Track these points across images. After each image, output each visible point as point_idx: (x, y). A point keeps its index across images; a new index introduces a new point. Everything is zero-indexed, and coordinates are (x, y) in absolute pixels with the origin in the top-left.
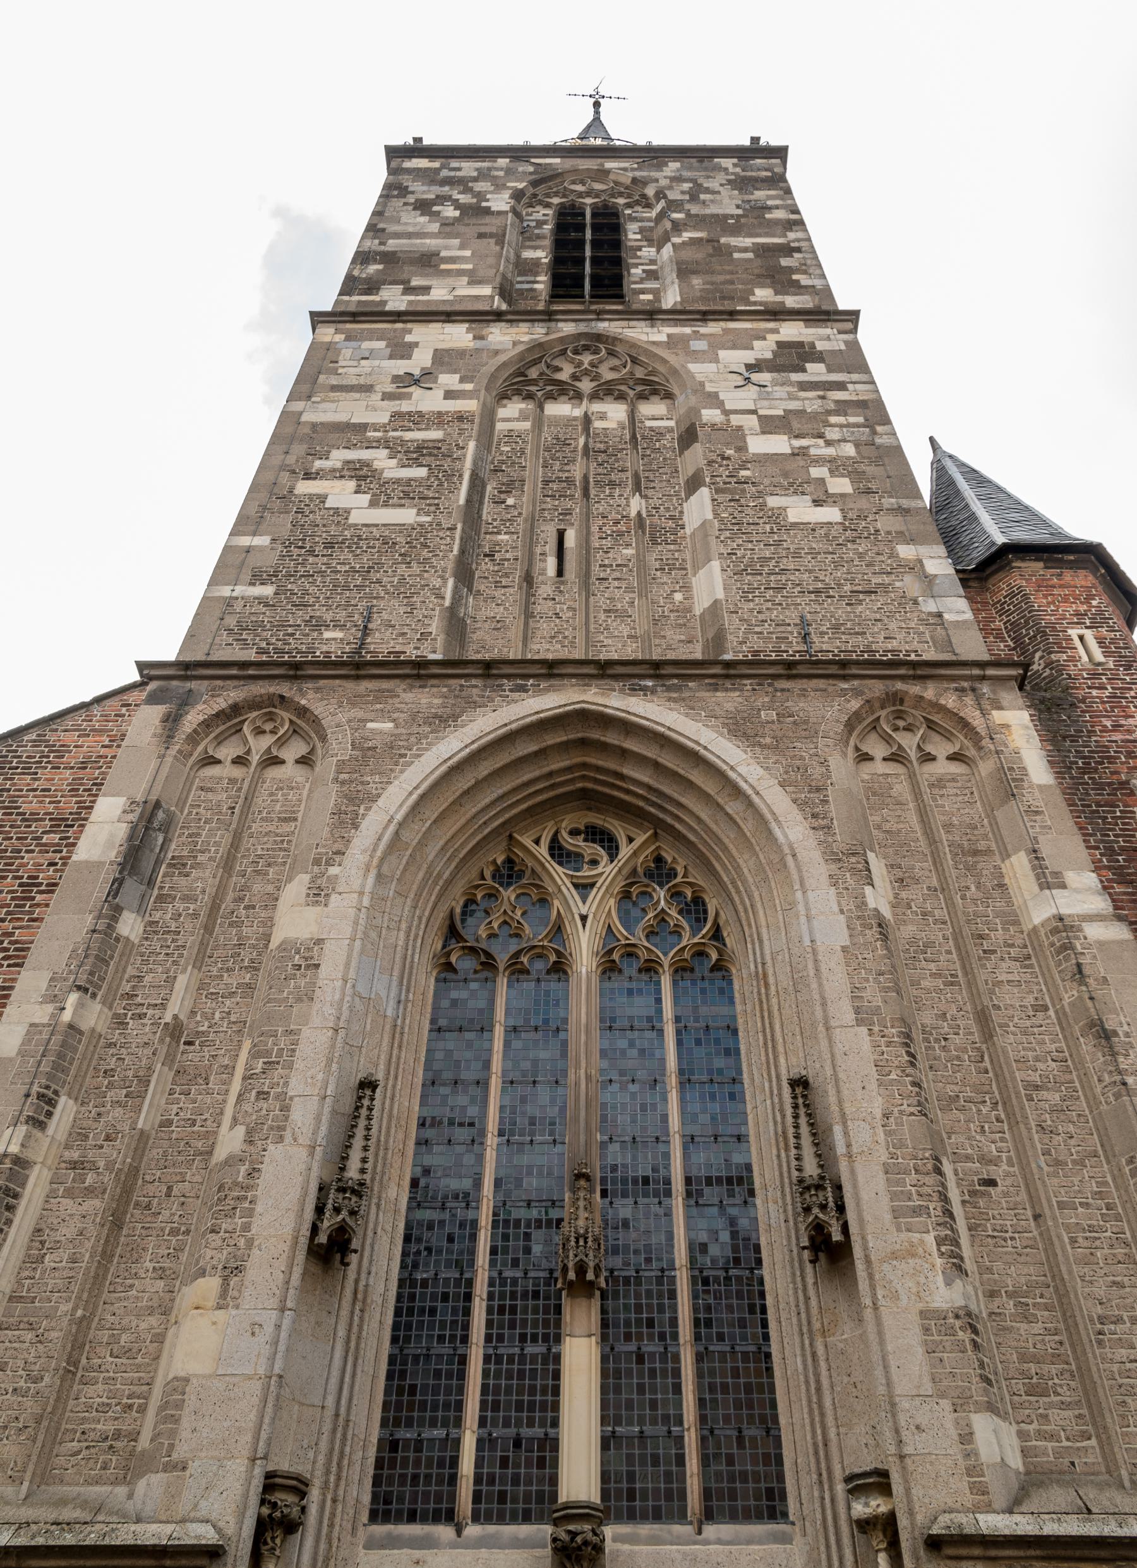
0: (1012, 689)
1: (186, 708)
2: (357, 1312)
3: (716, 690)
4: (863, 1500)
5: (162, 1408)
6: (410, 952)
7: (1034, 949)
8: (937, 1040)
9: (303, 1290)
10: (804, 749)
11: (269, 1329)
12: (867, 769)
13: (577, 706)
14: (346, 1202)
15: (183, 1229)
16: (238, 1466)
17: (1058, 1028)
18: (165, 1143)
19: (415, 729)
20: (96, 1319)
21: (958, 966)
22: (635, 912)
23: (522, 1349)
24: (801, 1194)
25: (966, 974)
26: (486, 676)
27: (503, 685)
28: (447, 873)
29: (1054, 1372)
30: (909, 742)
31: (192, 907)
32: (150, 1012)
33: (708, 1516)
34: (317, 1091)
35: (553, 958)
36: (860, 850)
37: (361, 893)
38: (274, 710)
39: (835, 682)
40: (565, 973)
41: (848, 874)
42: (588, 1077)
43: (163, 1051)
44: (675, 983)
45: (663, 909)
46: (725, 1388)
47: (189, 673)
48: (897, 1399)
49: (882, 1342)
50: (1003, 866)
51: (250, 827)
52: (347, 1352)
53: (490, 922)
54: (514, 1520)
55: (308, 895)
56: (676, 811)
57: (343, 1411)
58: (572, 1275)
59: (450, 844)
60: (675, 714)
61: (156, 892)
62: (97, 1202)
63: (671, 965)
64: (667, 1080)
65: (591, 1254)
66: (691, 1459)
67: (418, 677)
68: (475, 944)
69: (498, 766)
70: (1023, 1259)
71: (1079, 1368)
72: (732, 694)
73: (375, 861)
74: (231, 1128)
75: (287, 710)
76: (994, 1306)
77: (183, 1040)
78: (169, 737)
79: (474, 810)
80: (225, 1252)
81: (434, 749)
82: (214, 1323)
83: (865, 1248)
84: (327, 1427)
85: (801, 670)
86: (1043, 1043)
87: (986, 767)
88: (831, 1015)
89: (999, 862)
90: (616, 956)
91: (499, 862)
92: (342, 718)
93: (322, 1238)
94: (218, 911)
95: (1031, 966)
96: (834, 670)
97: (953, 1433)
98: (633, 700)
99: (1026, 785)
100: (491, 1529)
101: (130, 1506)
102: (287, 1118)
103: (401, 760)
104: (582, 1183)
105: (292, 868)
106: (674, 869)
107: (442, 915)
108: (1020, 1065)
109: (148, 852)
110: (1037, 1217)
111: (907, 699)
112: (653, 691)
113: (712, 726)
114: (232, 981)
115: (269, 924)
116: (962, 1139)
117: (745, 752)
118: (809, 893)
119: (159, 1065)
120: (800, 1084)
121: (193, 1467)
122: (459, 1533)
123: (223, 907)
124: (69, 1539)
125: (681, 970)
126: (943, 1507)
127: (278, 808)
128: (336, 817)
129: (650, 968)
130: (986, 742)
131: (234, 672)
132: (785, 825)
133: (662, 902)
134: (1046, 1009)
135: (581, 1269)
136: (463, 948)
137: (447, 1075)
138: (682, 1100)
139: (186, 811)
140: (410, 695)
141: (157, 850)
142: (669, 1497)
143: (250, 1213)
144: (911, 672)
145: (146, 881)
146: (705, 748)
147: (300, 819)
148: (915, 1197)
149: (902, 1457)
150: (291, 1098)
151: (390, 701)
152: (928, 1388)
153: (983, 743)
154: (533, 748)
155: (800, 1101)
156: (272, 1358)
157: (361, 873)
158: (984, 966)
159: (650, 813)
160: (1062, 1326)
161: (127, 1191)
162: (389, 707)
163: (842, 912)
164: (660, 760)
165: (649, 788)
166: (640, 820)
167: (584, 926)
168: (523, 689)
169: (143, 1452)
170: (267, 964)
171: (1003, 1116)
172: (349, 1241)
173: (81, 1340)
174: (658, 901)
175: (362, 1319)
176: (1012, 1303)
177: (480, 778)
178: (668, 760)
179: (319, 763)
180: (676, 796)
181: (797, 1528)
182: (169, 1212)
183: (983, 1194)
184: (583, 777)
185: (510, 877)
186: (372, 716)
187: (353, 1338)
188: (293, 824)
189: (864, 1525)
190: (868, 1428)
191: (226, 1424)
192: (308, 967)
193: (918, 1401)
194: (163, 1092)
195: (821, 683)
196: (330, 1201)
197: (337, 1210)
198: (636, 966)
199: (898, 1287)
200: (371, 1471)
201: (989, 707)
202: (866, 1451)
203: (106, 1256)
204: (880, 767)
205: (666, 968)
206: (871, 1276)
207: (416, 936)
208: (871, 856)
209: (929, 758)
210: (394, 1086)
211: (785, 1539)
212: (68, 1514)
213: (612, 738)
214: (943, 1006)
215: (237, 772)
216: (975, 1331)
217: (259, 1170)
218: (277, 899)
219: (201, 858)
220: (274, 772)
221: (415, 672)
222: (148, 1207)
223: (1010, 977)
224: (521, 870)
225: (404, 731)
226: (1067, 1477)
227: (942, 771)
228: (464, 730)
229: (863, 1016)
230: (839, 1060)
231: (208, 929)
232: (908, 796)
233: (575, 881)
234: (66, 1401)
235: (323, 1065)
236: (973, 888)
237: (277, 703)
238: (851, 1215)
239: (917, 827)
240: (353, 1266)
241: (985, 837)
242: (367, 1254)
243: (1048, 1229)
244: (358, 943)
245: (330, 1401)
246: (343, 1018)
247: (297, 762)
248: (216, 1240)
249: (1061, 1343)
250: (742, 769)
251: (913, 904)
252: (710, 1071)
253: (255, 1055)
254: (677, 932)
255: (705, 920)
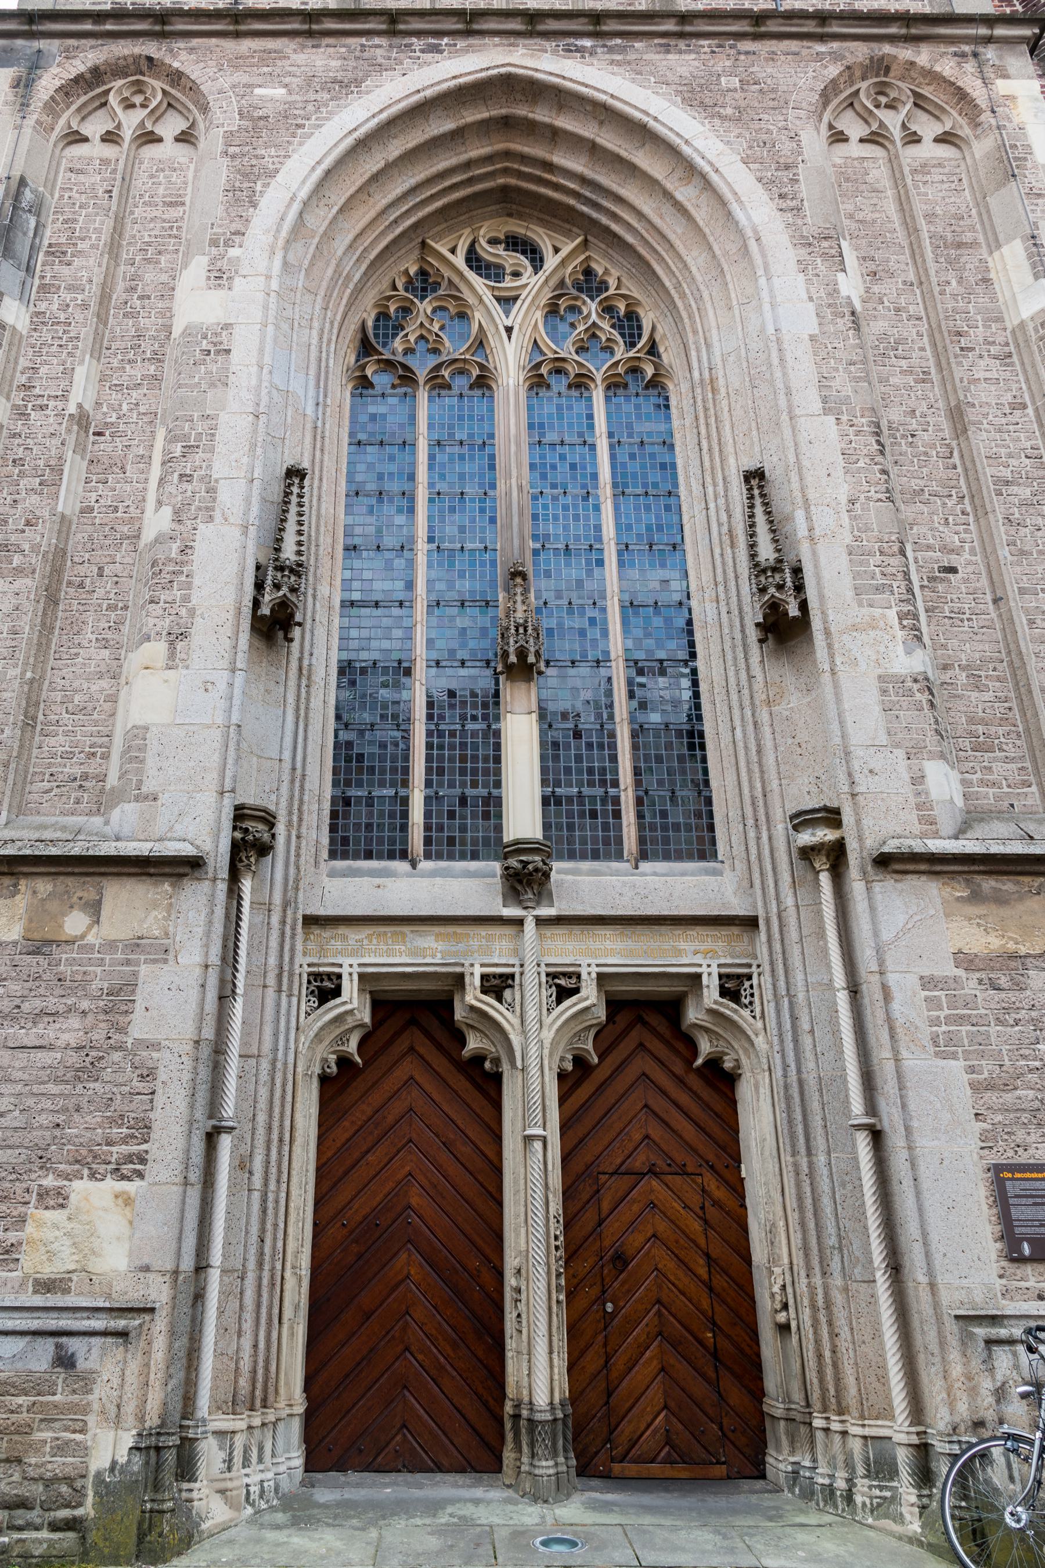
0: (1022, 54)
1: (38, 72)
2: (303, 685)
3: (668, 52)
4: (810, 831)
5: (124, 753)
6: (324, 354)
7: (1018, 346)
8: (903, 436)
9: (250, 661)
10: (772, 122)
11: (222, 686)
12: (841, 149)
13: (503, 70)
14: (286, 579)
15: (120, 605)
16: (209, 797)
17: (1035, 426)
18: (90, 528)
19: (312, 96)
20: (47, 682)
21: (931, 363)
22: (563, 327)
23: (463, 726)
24: (757, 576)
25: (940, 369)
26: (392, 33)
27: (412, 44)
28: (357, 276)
29: (1001, 733)
30: (892, 120)
31: (80, 297)
32: (52, 404)
33: (644, 855)
34: (243, 475)
35: (475, 372)
36: (833, 233)
37: (268, 277)
38: (141, 78)
39: (810, 44)
40: (490, 388)
41: (819, 260)
42: (520, 488)
43: (71, 440)
44: (607, 399)
45: (594, 323)
46: (659, 759)
47: (34, 28)
48: (852, 748)
49: (838, 700)
50: (989, 259)
51: (132, 213)
52: (297, 718)
53: (406, 335)
54: (463, 857)
55: (209, 278)
56: (613, 208)
57: (299, 765)
58: (513, 659)
59: (359, 242)
60: (618, 80)
61: (37, 282)
62: (28, 581)
63: (604, 380)
64: (600, 492)
65: (531, 640)
66: (628, 812)
67: (310, 34)
68: (392, 357)
69: (410, 145)
70: (978, 638)
71: (1027, 730)
72: (687, 57)
73: (281, 243)
74: (156, 511)
75: (157, 77)
76: (946, 677)
77: (91, 431)
78: (23, 105)
79: (385, 202)
80: (167, 620)
81: (336, 118)
82: (166, 681)
83: (825, 622)
84: (286, 777)
85: (772, 26)
86: (1019, 440)
87: (981, 148)
88: (796, 403)
89: (985, 256)
90: (544, 370)
91: (412, 272)
92: (225, 81)
93: (265, 610)
94: (110, 301)
95: (1012, 364)
96: (810, 27)
97: (906, 777)
98: (569, 62)
99: (1029, 164)
100: (443, 864)
101: (107, 830)
102: (214, 500)
103: (299, 131)
104: (519, 580)
105: (186, 254)
106: (605, 282)
107: (353, 327)
108: (990, 461)
109: (20, 234)
110: (996, 601)
111: (894, 67)
112: (592, 53)
113: (663, 94)
114: (136, 372)
115: (168, 314)
116: (924, 530)
117: (703, 124)
118: (775, 280)
119: (71, 452)
120: (755, 477)
121: (163, 798)
122: (414, 866)
123: (114, 297)
124: (54, 851)
125: (614, 385)
126: (892, 833)
127: (161, 191)
128: (231, 194)
129: (581, 383)
130: (986, 117)
131: (88, 27)
132: (748, 205)
133: (594, 316)
134: (1024, 407)
135: (522, 653)
136: (379, 361)
137: (372, 487)
138: (616, 508)
139: (57, 196)
140: (302, 56)
141: (31, 234)
142: (607, 842)
143: (189, 586)
144: (903, 31)
145: (24, 267)
146: (656, 119)
147: (188, 203)
148: (878, 576)
149: (854, 795)
150: (217, 481)
151: (279, 63)
152: (883, 739)
153: (982, 118)
154: (449, 126)
155: (756, 492)
156: (229, 710)
157: (266, 254)
158: (959, 364)
159: (582, 214)
160: (1012, 695)
161: (56, 572)
162: (278, 70)
163: (811, 299)
164: (598, 140)
165: (583, 180)
166: (568, 226)
167: (509, 338)
168: (436, 49)
169: (113, 788)
170: (172, 352)
171: (969, 509)
172: (292, 615)
173: (34, 699)
174: (589, 315)
175: (308, 693)
176: (964, 675)
177: (391, 159)
178: (609, 140)
179: (202, 138)
180: (615, 187)
181: (726, 866)
182: (104, 589)
183: (942, 580)
184: (506, 171)
185: (424, 289)
186: (259, 80)
187: (302, 707)
188: (181, 209)
189: (807, 853)
190: (812, 779)
191: (192, 764)
192: (218, 352)
193: (872, 750)
194: (78, 480)
195: (793, 45)
196: (269, 578)
197: (277, 587)
198: (565, 382)
199: (858, 655)
200: (327, 821)
201: (992, 76)
202: (807, 797)
203: (46, 628)
204: (854, 149)
205: (599, 381)
206: (830, 646)
207: (329, 341)
208: (844, 244)
209: (914, 139)
210: (320, 488)
211: (720, 873)
212: (47, 835)
213: (542, 115)
214: (912, 403)
215: (109, 151)
216: (932, 694)
217: (191, 547)
218: (173, 289)
219: (81, 246)
220: (150, 152)
221: (306, 27)
222: (81, 585)
223: (988, 375)
224: (435, 283)
225: (298, 98)
226: (1006, 816)
227: (928, 155)
228: (370, 97)
229: (830, 406)
230: (804, 448)
231: (102, 318)
232: (886, 183)
233: (496, 293)
234: (30, 750)
235: (246, 449)
236: (954, 283)
237: (145, 68)
238: (811, 593)
239: (895, 217)
240: (295, 645)
241: (972, 228)
242: (308, 626)
243: (1010, 610)
244: (270, 328)
245: (287, 755)
246: (263, 404)
247: (177, 140)
248: (156, 609)
249: (1010, 709)
250: (698, 143)
251: (885, 299)
252: (645, 485)
253: (172, 438)
254: (609, 350)
255: (640, 336)
